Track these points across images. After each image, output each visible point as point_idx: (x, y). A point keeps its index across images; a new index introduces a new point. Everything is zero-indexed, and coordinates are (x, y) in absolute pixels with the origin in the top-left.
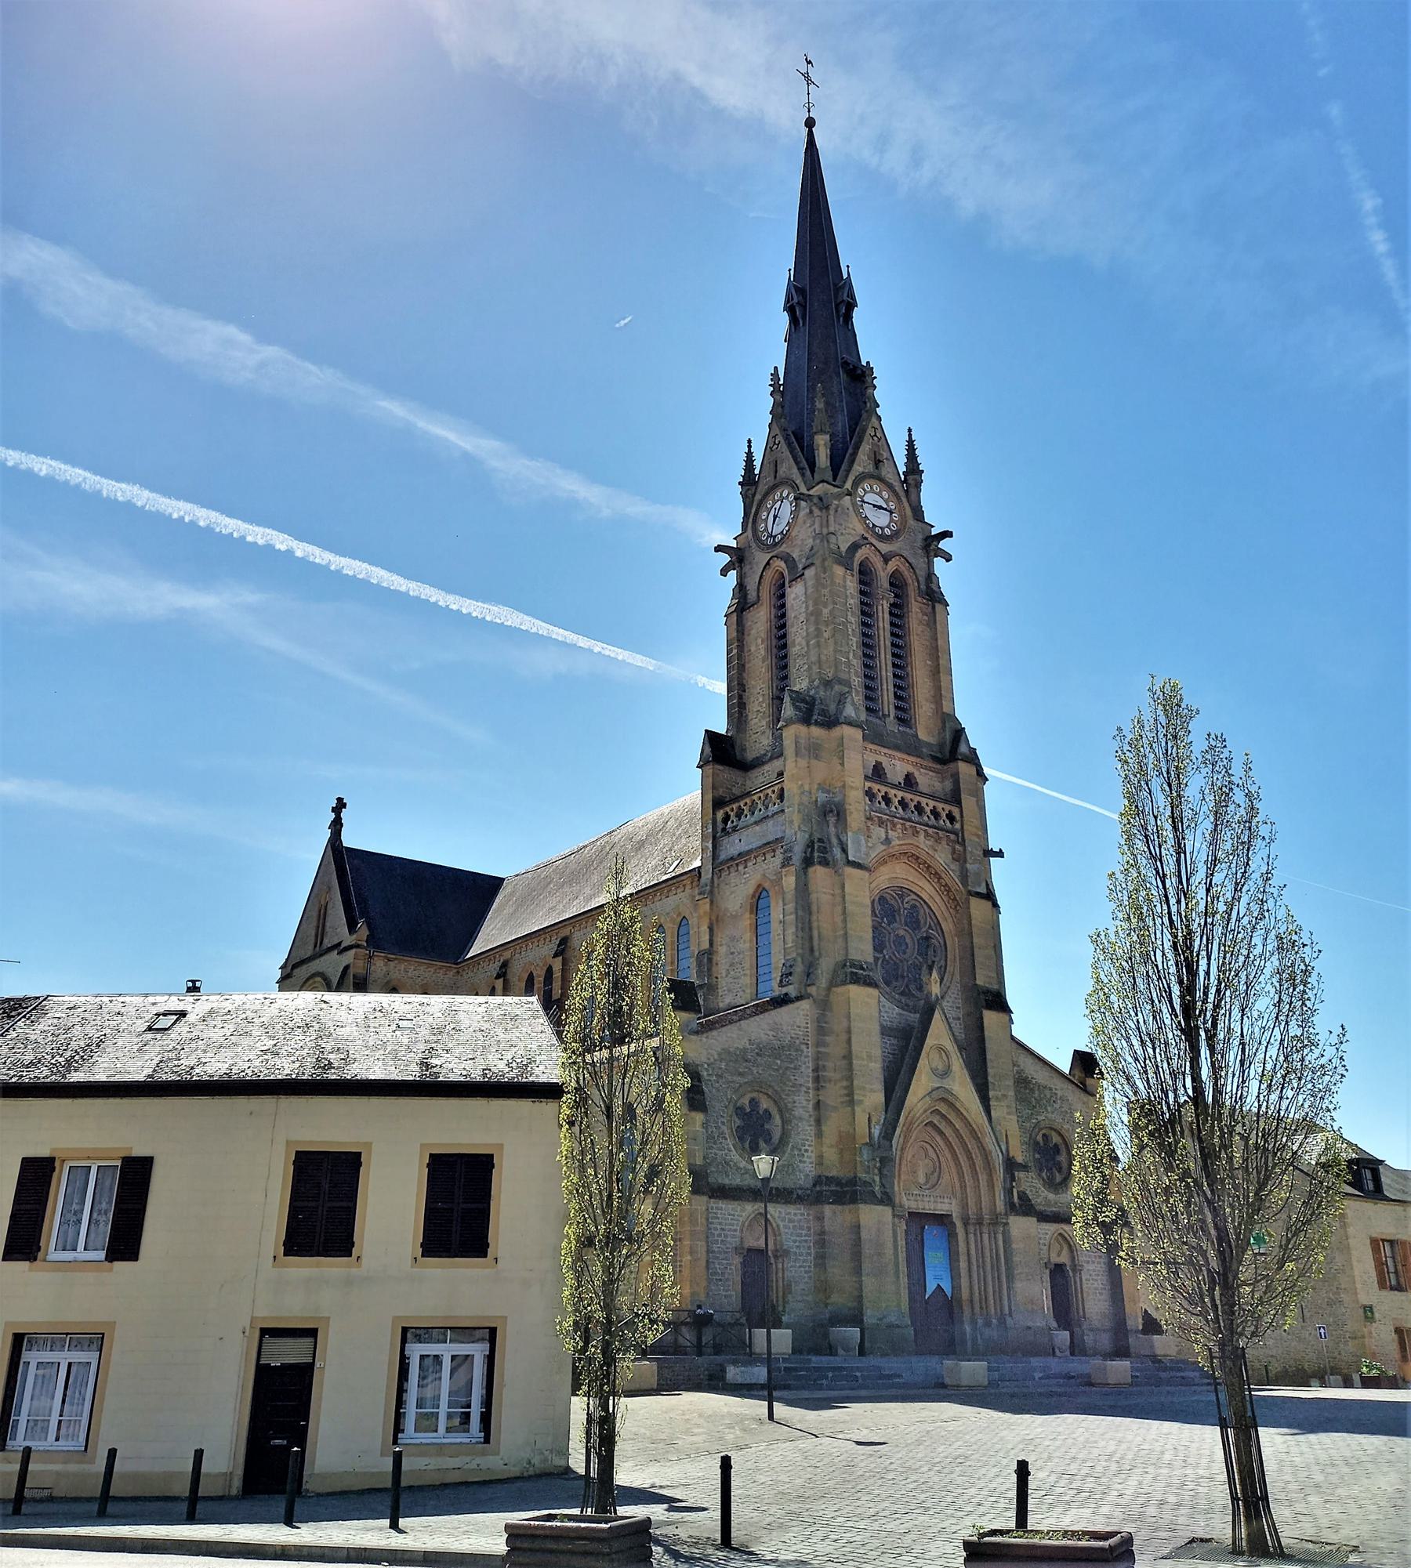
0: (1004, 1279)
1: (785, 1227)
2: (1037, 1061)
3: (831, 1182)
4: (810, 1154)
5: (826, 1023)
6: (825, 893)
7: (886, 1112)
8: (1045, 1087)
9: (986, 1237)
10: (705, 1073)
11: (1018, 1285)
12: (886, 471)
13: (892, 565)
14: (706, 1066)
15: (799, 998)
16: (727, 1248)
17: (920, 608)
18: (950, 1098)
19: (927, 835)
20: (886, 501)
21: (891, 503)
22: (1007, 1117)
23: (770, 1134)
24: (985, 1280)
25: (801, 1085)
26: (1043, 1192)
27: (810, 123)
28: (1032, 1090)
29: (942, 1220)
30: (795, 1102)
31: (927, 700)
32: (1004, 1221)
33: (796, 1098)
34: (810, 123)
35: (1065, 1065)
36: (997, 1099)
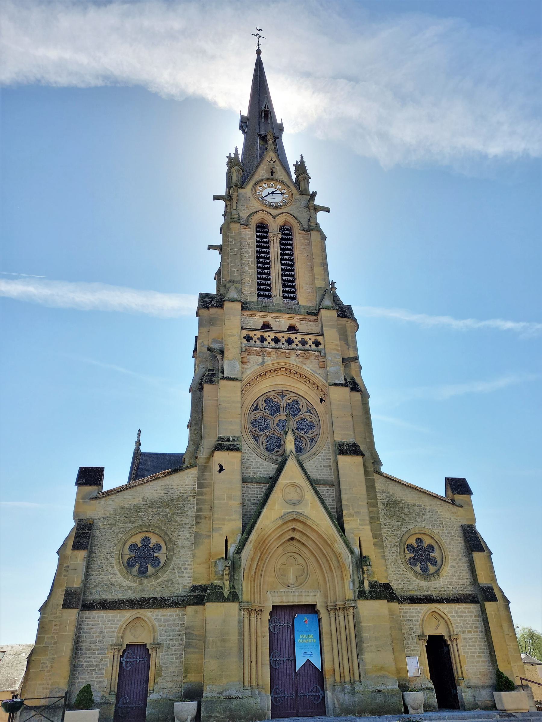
0: (354, 651)
1: (160, 626)
2: (405, 488)
3: (198, 589)
4: (188, 571)
5: (204, 480)
6: (210, 400)
7: (242, 534)
8: (414, 505)
11: (368, 657)
12: (280, 174)
13: (280, 220)
14: (102, 519)
16: (105, 646)
17: (303, 237)
18: (301, 518)
20: (279, 190)
21: (278, 186)
22: (361, 527)
23: (159, 560)
24: (351, 651)
25: (185, 524)
27: (259, 52)
29: (311, 609)
31: (307, 284)
32: (353, 605)
33: (180, 533)
34: (259, 52)
35: (441, 490)
36: (351, 515)
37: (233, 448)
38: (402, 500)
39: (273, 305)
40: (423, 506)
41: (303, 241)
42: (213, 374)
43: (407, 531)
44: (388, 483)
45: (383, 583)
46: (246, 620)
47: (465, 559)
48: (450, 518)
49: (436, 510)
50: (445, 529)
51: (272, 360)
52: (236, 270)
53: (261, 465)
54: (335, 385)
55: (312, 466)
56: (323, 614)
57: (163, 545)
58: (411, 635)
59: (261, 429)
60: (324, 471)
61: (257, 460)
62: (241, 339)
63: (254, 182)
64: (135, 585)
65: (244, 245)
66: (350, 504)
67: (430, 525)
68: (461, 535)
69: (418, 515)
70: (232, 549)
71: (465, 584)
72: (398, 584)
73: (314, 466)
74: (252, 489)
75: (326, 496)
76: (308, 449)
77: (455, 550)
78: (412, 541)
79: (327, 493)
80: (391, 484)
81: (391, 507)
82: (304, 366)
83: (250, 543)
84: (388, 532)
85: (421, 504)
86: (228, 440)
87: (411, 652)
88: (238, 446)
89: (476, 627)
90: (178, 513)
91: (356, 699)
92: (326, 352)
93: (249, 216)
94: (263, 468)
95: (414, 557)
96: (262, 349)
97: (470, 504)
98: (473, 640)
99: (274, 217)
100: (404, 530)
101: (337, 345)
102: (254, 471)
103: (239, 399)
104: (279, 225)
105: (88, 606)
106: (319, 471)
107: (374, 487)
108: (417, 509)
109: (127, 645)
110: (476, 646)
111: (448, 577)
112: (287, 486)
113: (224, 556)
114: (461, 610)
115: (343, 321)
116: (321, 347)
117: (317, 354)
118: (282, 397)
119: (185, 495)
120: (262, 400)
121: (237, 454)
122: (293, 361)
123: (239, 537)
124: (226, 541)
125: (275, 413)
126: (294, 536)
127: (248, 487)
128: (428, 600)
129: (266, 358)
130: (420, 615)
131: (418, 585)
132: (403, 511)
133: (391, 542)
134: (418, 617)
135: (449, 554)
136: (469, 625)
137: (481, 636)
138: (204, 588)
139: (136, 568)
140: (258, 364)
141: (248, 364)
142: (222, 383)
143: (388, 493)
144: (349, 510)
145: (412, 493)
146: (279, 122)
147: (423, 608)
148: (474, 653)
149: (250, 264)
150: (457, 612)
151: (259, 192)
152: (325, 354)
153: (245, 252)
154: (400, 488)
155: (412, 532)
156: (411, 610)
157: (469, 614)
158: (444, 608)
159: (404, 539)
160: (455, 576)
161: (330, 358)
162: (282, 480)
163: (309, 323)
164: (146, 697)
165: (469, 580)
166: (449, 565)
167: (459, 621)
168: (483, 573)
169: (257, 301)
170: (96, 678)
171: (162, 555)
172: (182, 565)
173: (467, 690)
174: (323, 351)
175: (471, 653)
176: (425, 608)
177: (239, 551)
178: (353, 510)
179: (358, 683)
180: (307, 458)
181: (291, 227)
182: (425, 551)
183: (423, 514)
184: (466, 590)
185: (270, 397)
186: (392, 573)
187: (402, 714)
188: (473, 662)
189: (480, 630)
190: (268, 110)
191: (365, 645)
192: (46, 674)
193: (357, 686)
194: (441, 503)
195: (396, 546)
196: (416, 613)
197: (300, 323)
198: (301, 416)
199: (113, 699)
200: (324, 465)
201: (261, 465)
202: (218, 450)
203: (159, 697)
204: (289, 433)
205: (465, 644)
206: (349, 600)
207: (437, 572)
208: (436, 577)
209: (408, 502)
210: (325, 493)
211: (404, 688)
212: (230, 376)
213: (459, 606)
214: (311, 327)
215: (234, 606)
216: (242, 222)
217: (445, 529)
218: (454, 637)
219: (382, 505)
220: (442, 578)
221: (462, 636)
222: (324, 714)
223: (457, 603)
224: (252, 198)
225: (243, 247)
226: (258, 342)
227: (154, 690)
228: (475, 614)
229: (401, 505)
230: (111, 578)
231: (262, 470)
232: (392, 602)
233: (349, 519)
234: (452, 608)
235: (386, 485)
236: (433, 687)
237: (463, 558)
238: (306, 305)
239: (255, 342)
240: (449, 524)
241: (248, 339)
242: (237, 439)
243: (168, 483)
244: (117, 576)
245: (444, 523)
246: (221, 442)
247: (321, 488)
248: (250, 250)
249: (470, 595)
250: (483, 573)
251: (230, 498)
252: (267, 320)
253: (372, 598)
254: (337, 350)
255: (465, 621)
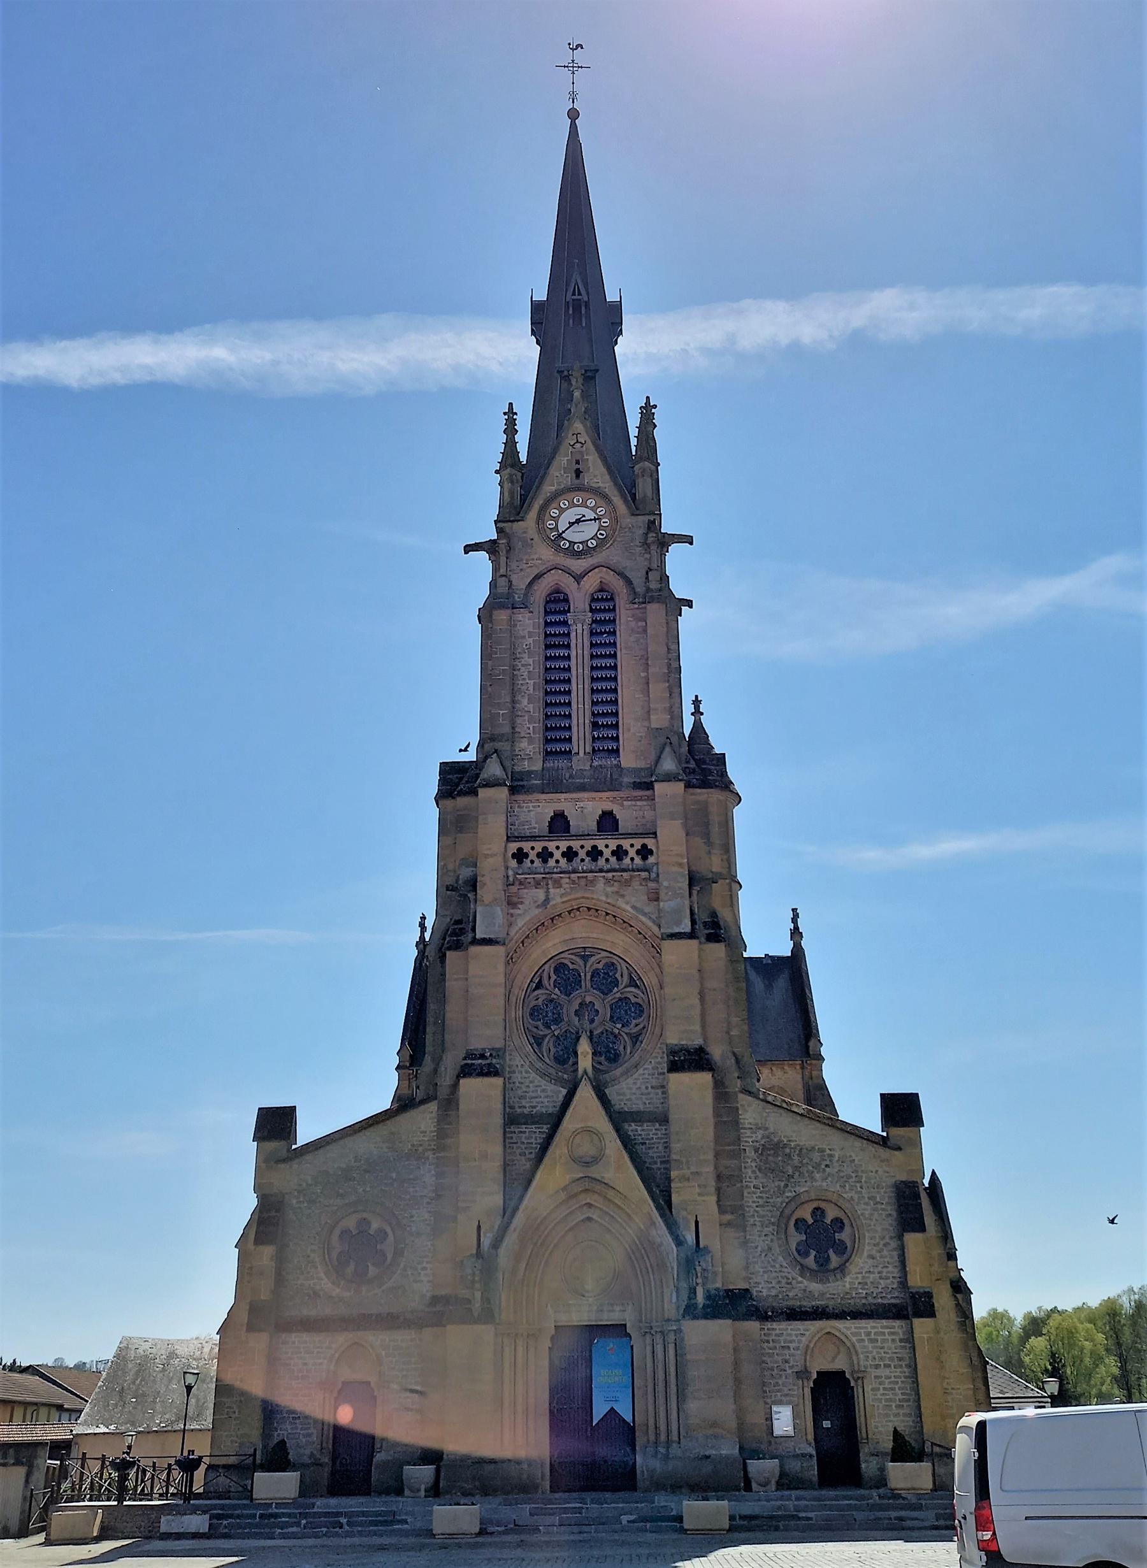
2: (799, 1118)
6: (456, 980)
9: (520, 1350)
10: (294, 1201)
11: (692, 1406)
13: (591, 583)
14: (296, 1193)
15: (423, 1102)
17: (633, 616)
19: (607, 881)
20: (593, 509)
26: (801, 1282)
27: (573, 115)
28: (789, 1156)
29: (619, 1330)
30: (412, 1217)
32: (675, 1328)
33: (414, 1212)
34: (573, 115)
37: (490, 1071)
38: (790, 1141)
39: (571, 777)
40: (828, 1152)
41: (633, 624)
42: (461, 929)
43: (795, 1196)
44: (767, 1111)
45: (739, 1289)
46: (507, 1351)
47: (894, 1244)
48: (877, 1171)
49: (851, 1156)
50: (864, 1191)
51: (562, 896)
52: (501, 712)
53: (543, 1091)
54: (672, 936)
55: (630, 1089)
56: (636, 1341)
57: (389, 1230)
58: (785, 1370)
59: (547, 1023)
60: (651, 1096)
61: (536, 1083)
62: (505, 860)
63: (541, 502)
64: (348, 1294)
65: (519, 651)
66: (684, 1160)
67: (838, 1185)
68: (894, 1200)
69: (817, 1166)
70: (486, 1242)
71: (890, 1287)
72: (770, 1288)
73: (635, 1087)
74: (527, 1134)
75: (652, 1141)
76: (627, 1057)
77: (879, 1229)
78: (806, 1213)
79: (655, 1137)
80: (774, 1112)
81: (769, 1155)
82: (621, 903)
83: (515, 1230)
84: (759, 1200)
85: (825, 1147)
86: (482, 1056)
87: (783, 1398)
88: (498, 1066)
89: (900, 1359)
90: (410, 1179)
91: (670, 1468)
92: (660, 871)
93: (531, 584)
94: (547, 1097)
95: (806, 1241)
96: (544, 876)
97: (917, 1144)
98: (893, 1379)
99: (578, 578)
100: (789, 1194)
101: (681, 856)
102: (531, 1102)
103: (501, 979)
104: (588, 595)
105: (286, 1326)
106: (644, 1097)
107: (736, 1124)
108: (816, 1157)
109: (343, 1382)
110: (897, 1389)
111: (860, 1276)
112: (576, 1133)
113: (474, 1252)
114: (876, 1330)
115: (702, 794)
116: (651, 860)
117: (644, 874)
118: (585, 958)
119: (420, 1149)
120: (549, 968)
121: (498, 1081)
122: (601, 892)
123: (498, 1222)
124: (479, 1227)
125: (573, 989)
126: (591, 1216)
127: (521, 1132)
128: (819, 1314)
129: (551, 890)
130: (804, 1339)
131: (805, 1291)
132: (790, 1162)
133: (763, 1216)
134: (800, 1342)
135: (867, 1234)
136: (888, 1356)
137: (907, 1374)
138: (446, 1300)
139: (350, 1269)
140: (538, 905)
141: (520, 906)
142: (474, 950)
143: (767, 1129)
144: (682, 1169)
145: (810, 1126)
146: (612, 296)
147: (810, 1327)
148: (890, 1400)
149: (531, 692)
150: (869, 1334)
151: (552, 522)
152: (658, 875)
153: (523, 665)
154: (790, 1119)
155: (803, 1198)
156: (789, 1331)
157: (890, 1338)
158: (845, 1327)
159: (787, 1212)
160: (873, 1273)
161: (665, 884)
162: (569, 1123)
163: (639, 803)
164: (373, 1456)
165: (899, 1280)
166: (865, 1254)
167: (870, 1349)
168: (918, 1270)
169: (543, 769)
170: (301, 1429)
171: (388, 1247)
172: (418, 1264)
173: (872, 1458)
174: (655, 869)
175: (886, 1400)
176: (813, 1328)
177: (496, 1244)
178: (689, 1168)
179: (674, 1445)
180: (622, 1075)
181: (612, 594)
182: (826, 1230)
183: (827, 1166)
184: (889, 1296)
185: (563, 961)
186: (762, 1270)
187: (739, 1490)
188: (887, 1415)
189: (906, 1363)
190: (579, 297)
191: (690, 1389)
192: (234, 1422)
193: (675, 1450)
194: (862, 1144)
195: (773, 1224)
196: (796, 1335)
197: (622, 805)
198: (618, 995)
199: (326, 1460)
200: (654, 1084)
201: (543, 1091)
202: (464, 1077)
203: (390, 1458)
204: (581, 1039)
205: (878, 1386)
206: (669, 1320)
207: (842, 1269)
208: (838, 1276)
209: (801, 1144)
210: (651, 1136)
211: (749, 1452)
212: (485, 936)
213: (874, 1324)
214: (641, 813)
215: (486, 1332)
216: (519, 598)
217: (864, 1191)
218: (860, 1375)
219: (753, 1152)
220: (848, 1277)
221: (874, 1372)
222: (634, 1488)
223: (869, 1318)
224: (536, 537)
225: (518, 656)
226: (538, 863)
227: (381, 1447)
228: (902, 1336)
229: (787, 1151)
230: (314, 1284)
231: (546, 1100)
232: (747, 1320)
233: (680, 1185)
234: (860, 1328)
235: (765, 1114)
236: (814, 1453)
237: (891, 1242)
238: (634, 766)
239: (532, 862)
240: (873, 1182)
241: (520, 856)
242: (498, 1053)
243: (393, 1130)
244: (323, 1282)
245: (863, 1181)
246: (469, 1062)
247: (645, 1128)
248: (531, 661)
249: (895, 1305)
250: (918, 1270)
251: (484, 1156)
252: (559, 807)
253: (706, 1316)
254: (681, 865)
255: (882, 1348)
